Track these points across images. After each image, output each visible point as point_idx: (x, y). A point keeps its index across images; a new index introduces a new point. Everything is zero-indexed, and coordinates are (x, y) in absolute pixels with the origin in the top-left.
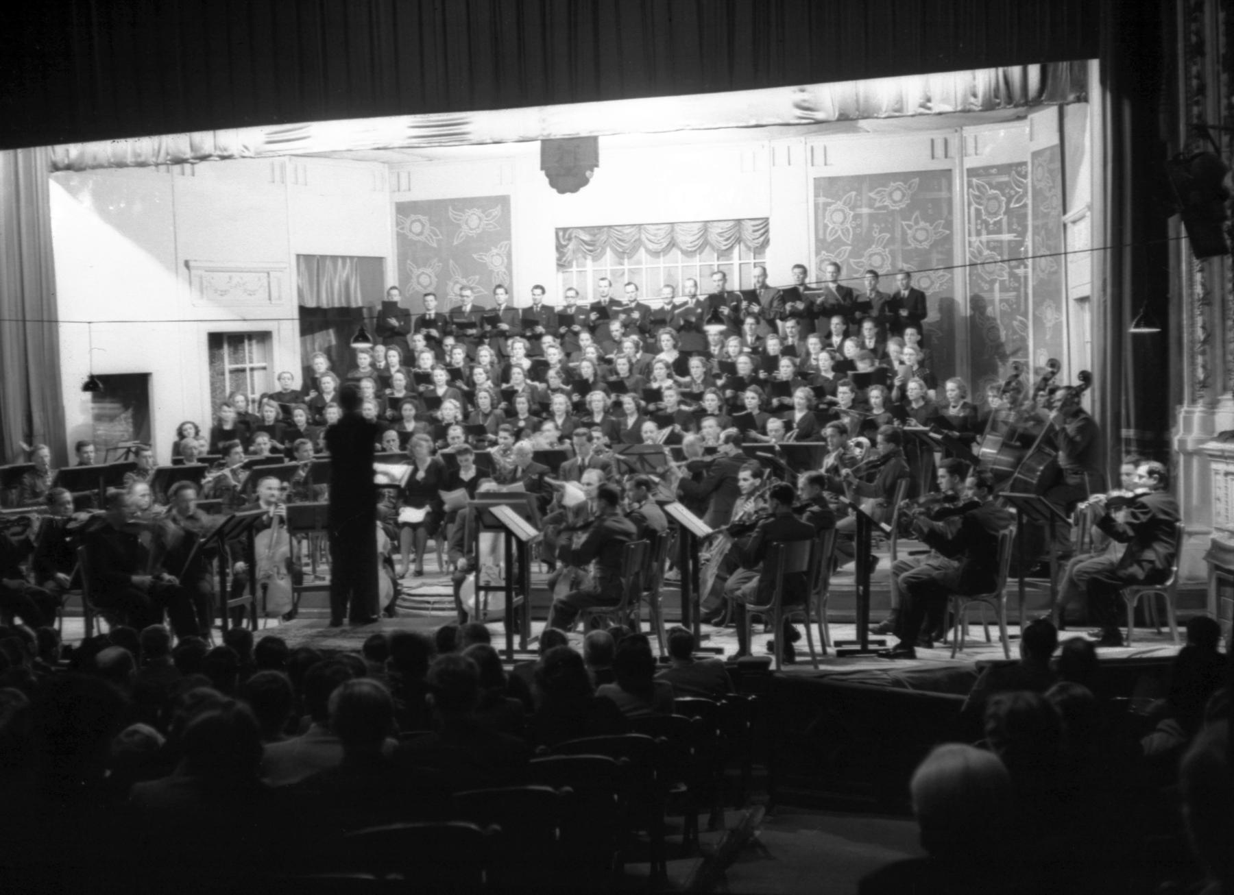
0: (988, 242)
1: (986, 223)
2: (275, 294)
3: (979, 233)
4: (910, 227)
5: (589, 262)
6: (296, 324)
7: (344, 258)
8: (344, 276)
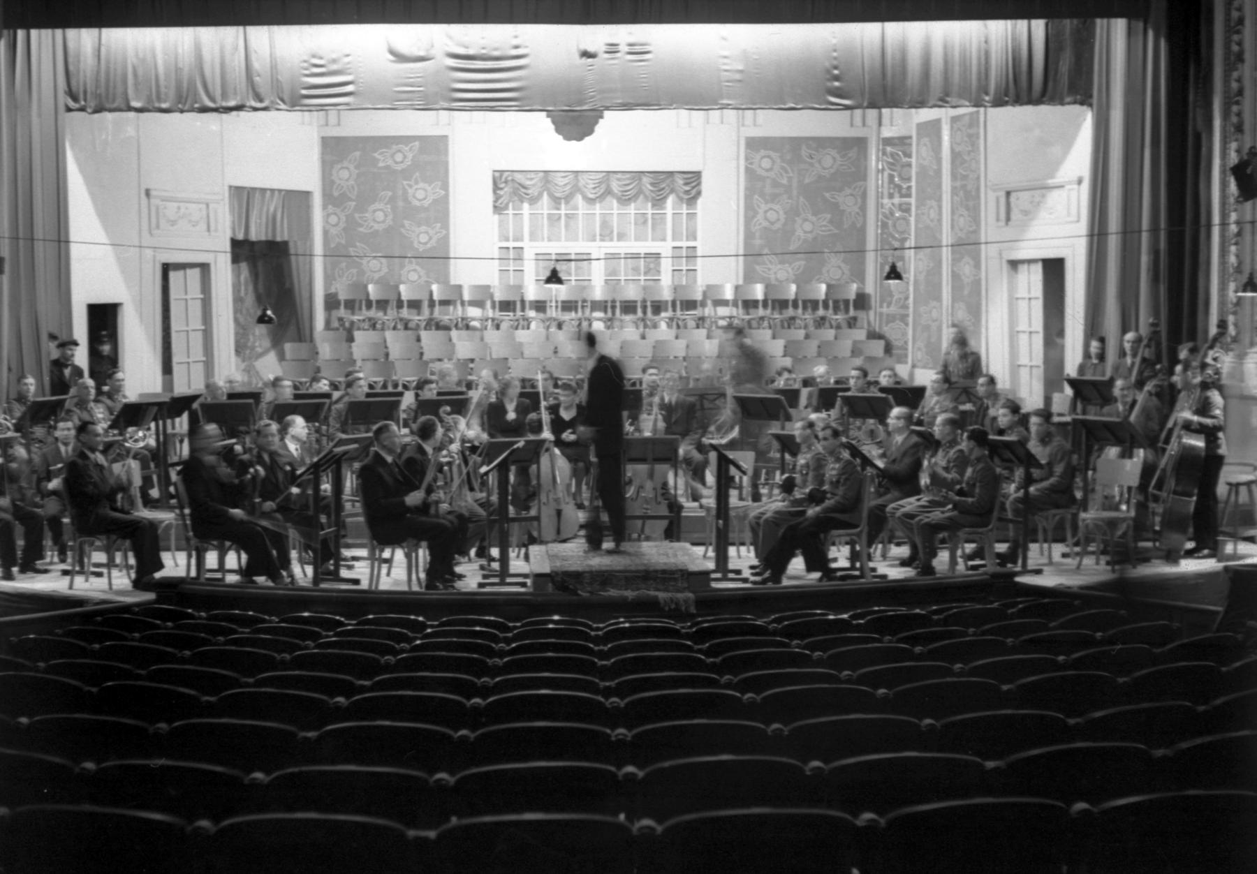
0: (900, 205)
1: (899, 187)
2: (212, 228)
3: (891, 196)
4: (411, 186)
5: (526, 205)
6: (229, 256)
7: (272, 191)
8: (272, 209)
